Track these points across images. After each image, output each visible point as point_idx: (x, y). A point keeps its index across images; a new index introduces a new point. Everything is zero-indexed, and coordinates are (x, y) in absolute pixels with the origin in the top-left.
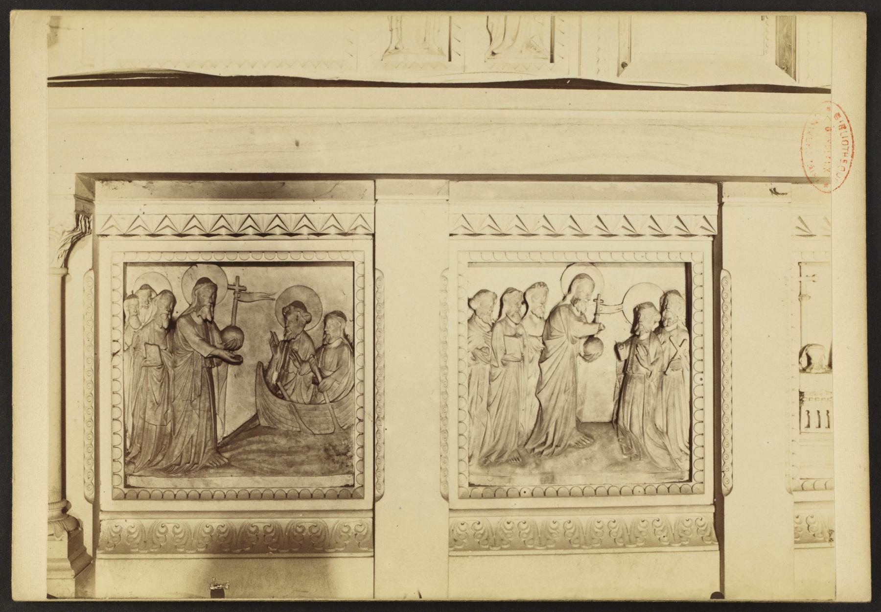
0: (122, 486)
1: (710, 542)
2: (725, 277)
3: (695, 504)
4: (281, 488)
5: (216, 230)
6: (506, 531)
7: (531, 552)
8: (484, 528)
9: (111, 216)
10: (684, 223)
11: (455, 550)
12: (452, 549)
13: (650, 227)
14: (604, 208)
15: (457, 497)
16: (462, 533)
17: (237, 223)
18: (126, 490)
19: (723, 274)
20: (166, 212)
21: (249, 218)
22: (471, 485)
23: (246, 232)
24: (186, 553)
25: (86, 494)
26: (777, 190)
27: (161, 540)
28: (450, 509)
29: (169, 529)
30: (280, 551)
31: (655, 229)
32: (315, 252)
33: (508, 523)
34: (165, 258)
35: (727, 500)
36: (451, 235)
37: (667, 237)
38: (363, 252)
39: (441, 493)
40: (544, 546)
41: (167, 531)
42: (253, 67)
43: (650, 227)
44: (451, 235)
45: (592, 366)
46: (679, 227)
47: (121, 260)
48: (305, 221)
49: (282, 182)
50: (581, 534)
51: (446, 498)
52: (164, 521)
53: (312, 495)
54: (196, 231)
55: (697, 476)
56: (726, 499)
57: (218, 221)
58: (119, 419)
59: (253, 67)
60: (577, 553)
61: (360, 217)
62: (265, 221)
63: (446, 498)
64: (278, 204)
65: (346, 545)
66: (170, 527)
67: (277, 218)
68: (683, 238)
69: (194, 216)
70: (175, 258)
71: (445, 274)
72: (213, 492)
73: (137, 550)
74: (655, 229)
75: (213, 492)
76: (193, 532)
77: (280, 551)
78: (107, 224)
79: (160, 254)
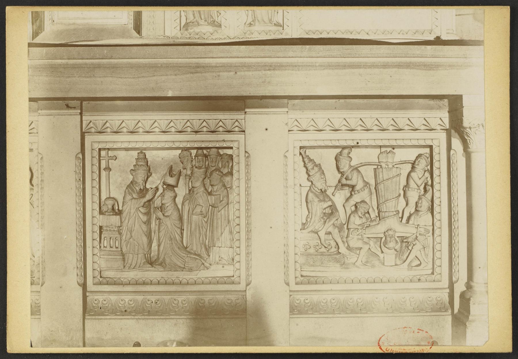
0: (99, 277)
1: (444, 310)
2: (453, 154)
3: (354, 289)
4: (206, 278)
5: (153, 129)
6: (120, 305)
7: (311, 316)
8: (215, 302)
9: (32, 122)
10: (380, 122)
11: (294, 314)
12: (292, 313)
13: (439, 124)
14: (365, 114)
15: (294, 283)
16: (297, 305)
17: (165, 125)
18: (101, 279)
19: (452, 152)
20: (140, 119)
21: (205, 122)
22: (302, 276)
23: (218, 130)
24: (313, 314)
25: (78, 281)
26: (70, 105)
27: (121, 308)
28: (290, 291)
29: (206, 300)
30: (368, 312)
31: (347, 126)
32: (232, 141)
33: (96, 300)
34: (329, 144)
35: (455, 285)
36: (289, 131)
37: (323, 131)
38: (238, 142)
39: (77, 282)
40: (114, 313)
41: (205, 302)
42: (430, 34)
43: (439, 124)
44: (289, 131)
45: (422, 207)
46: (330, 125)
47: (435, 144)
48: (237, 124)
49: (88, 102)
50: (341, 305)
51: (288, 284)
52: (123, 297)
53: (218, 282)
54: (173, 130)
55: (437, 270)
56: (455, 285)
57: (315, 122)
58: (97, 239)
59: (430, 34)
60: (298, 317)
61: (328, 120)
62: (116, 126)
63: (288, 284)
64: (121, 115)
65: (176, 311)
66: (302, 299)
67: (205, 122)
68: (334, 132)
69: (172, 121)
70: (188, 145)
71: (286, 154)
72: (218, 279)
73: (134, 314)
74: (347, 126)
75: (144, 280)
76: (316, 303)
77: (368, 312)
78: (379, 125)
79: (143, 143)
